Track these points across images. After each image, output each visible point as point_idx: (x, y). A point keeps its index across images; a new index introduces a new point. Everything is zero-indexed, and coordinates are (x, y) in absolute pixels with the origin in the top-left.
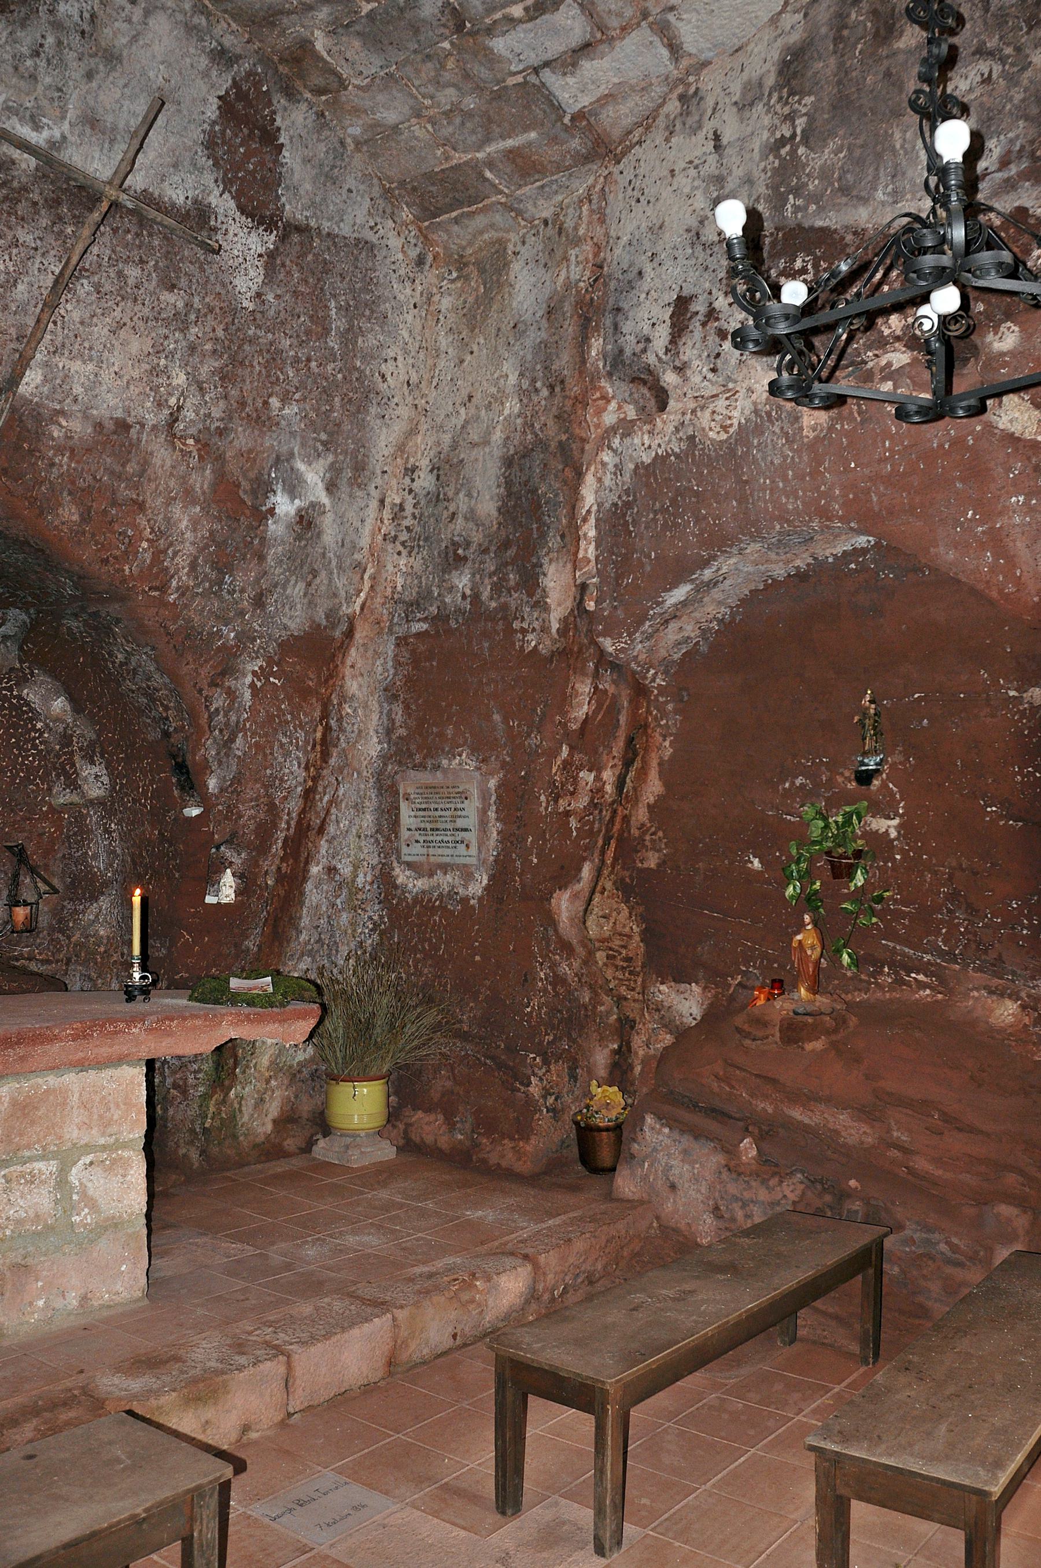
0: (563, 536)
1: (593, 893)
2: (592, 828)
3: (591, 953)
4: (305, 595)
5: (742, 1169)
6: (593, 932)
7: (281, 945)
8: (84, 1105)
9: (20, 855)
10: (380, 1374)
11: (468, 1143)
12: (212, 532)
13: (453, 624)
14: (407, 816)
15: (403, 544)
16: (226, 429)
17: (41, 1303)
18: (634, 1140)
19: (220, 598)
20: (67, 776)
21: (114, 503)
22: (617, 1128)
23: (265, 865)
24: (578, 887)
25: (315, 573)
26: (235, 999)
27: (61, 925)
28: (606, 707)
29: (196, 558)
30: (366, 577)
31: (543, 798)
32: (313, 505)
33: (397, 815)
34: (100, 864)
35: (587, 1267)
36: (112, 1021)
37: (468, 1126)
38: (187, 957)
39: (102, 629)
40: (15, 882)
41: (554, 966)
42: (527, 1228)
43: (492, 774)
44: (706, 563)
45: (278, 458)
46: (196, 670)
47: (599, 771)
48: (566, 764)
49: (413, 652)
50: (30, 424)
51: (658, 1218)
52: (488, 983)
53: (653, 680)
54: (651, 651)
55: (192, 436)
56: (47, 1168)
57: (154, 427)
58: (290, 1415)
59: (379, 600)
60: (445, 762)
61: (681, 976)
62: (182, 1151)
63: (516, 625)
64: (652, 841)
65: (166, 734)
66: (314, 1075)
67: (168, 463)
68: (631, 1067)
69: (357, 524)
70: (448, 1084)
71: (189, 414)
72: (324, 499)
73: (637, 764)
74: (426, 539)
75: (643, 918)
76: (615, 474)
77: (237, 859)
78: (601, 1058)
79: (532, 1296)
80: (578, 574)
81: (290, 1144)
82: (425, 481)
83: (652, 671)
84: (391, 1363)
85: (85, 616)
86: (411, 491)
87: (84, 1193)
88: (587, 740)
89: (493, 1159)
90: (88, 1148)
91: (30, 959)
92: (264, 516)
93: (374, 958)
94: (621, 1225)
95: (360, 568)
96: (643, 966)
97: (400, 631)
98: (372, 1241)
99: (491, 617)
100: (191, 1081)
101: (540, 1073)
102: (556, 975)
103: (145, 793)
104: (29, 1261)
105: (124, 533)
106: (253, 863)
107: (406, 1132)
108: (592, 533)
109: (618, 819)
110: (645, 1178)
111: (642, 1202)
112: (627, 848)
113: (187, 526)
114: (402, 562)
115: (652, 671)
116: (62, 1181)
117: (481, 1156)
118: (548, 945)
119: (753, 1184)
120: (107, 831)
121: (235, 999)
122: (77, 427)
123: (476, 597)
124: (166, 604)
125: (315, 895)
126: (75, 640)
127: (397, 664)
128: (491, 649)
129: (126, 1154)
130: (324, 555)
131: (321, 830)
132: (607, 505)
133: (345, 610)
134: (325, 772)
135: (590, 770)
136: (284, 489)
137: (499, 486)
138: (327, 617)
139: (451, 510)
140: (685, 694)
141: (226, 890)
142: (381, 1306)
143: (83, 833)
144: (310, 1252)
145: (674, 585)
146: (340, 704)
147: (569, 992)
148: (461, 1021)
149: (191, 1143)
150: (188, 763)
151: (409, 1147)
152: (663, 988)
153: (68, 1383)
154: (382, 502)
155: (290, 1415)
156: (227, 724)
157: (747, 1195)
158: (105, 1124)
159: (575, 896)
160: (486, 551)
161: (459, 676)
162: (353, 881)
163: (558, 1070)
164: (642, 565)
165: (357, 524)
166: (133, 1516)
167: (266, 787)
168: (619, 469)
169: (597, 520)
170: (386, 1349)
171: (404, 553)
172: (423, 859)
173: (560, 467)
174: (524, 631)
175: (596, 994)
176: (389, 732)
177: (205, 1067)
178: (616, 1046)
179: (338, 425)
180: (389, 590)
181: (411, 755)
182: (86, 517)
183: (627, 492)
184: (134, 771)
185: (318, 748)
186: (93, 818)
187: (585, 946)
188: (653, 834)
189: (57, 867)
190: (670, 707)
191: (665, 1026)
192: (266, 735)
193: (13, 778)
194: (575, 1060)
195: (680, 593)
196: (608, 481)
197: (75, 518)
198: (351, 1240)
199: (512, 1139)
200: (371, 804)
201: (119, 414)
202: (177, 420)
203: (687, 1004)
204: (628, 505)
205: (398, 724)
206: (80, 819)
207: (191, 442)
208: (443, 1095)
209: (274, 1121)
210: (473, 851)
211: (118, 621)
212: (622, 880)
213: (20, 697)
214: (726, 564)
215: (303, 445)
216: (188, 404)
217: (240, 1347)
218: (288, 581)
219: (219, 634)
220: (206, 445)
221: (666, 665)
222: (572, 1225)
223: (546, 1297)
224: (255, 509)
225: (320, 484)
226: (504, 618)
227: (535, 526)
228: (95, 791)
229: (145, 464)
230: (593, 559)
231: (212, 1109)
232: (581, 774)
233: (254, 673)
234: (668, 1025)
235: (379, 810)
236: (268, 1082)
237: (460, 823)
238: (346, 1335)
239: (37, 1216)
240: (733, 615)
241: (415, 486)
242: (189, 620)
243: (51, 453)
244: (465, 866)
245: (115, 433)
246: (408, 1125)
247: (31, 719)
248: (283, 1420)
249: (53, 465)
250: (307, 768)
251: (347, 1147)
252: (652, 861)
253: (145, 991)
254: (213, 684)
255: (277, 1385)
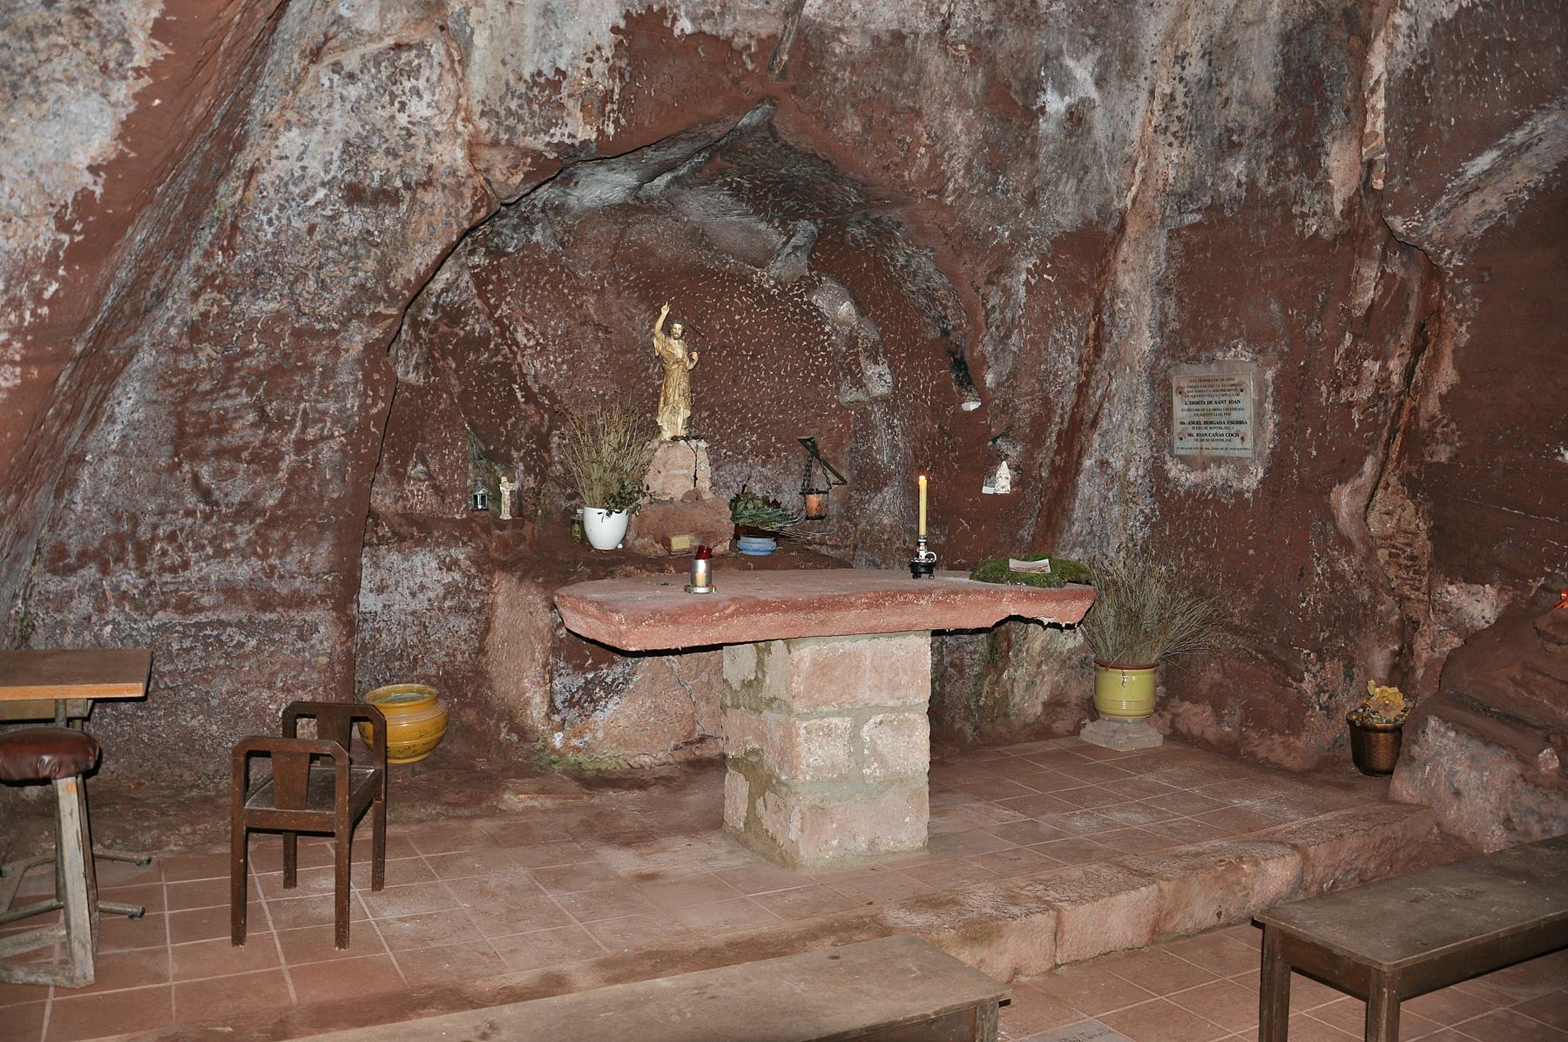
0: (1347, 112)
1: (1375, 488)
2: (1376, 421)
3: (1372, 551)
4: (1077, 191)
5: (1540, 780)
6: (1374, 528)
7: (1054, 535)
8: (875, 669)
9: (811, 447)
10: (1145, 940)
11: (1236, 736)
12: (985, 134)
13: (1228, 213)
14: (1180, 410)
15: (1174, 134)
16: (995, 31)
17: (835, 842)
18: (1415, 742)
19: (995, 198)
20: (854, 376)
21: (893, 112)
22: (1396, 731)
23: (1040, 458)
24: (1359, 482)
25: (1086, 169)
26: (1015, 577)
27: (848, 514)
28: (1394, 291)
29: (971, 160)
30: (1137, 171)
31: (1323, 388)
32: (1082, 101)
33: (1170, 409)
34: (884, 458)
35: (1359, 864)
36: (902, 592)
37: (1236, 719)
38: (972, 540)
39: (883, 234)
40: (808, 474)
41: (1331, 562)
42: (1296, 821)
43: (1268, 365)
44: (1517, 124)
45: (1047, 56)
46: (973, 269)
47: (1385, 361)
48: (1349, 353)
49: (1186, 244)
50: (814, 43)
51: (1438, 825)
52: (1261, 577)
53: (1449, 261)
54: (1447, 228)
55: (963, 42)
56: (842, 723)
57: (928, 36)
58: (1057, 966)
59: (1151, 193)
60: (1219, 354)
61: (1473, 576)
62: (957, 726)
63: (1296, 210)
64: (1443, 433)
65: (945, 332)
66: (1083, 663)
67: (942, 69)
68: (1413, 670)
69: (1127, 117)
70: (1218, 677)
71: (960, 21)
72: (1094, 94)
73: (1428, 352)
74: (1198, 128)
75: (1430, 515)
76: (1409, 36)
77: (1014, 451)
78: (1380, 659)
79: (1300, 884)
80: (1364, 150)
81: (1059, 726)
82: (1196, 68)
83: (1448, 251)
84: (1155, 931)
85: (869, 223)
86: (1181, 79)
87: (874, 749)
88: (1372, 329)
89: (1262, 753)
90: (879, 709)
91: (821, 544)
92: (1034, 114)
93: (1144, 550)
94: (1397, 827)
95: (1131, 161)
96: (1430, 565)
97: (1173, 224)
98: (1138, 819)
99: (1268, 204)
100: (967, 661)
101: (1314, 670)
102: (1334, 572)
103: (925, 389)
104: (826, 805)
105: (904, 140)
106: (1029, 455)
107: (1172, 722)
108: (1381, 105)
109: (1405, 412)
110: (1425, 782)
111: (1420, 806)
112: (1415, 441)
113: (961, 129)
114: (1174, 152)
115: (1448, 251)
116: (855, 737)
117: (1250, 749)
118: (1326, 540)
119: (1554, 798)
120: (890, 426)
121: (1015, 577)
122: (856, 42)
123: (1252, 184)
124: (944, 207)
125: (1087, 487)
126: (859, 246)
127: (1170, 257)
128: (1268, 236)
129: (912, 716)
130: (1094, 150)
131: (1094, 424)
132: (1399, 72)
133: (1117, 204)
134: (1097, 367)
135: (1375, 359)
136: (1053, 87)
137: (1276, 65)
138: (1099, 213)
139: (1225, 95)
140: (1485, 274)
141: (1002, 481)
142: (1148, 877)
143: (868, 427)
144: (1079, 824)
145: (1478, 152)
146: (1112, 300)
147: (1347, 589)
148: (1232, 615)
149: (966, 719)
150: (967, 359)
151: (1176, 736)
152: (1452, 588)
153: (861, 912)
154: (1152, 93)
155: (1057, 966)
156: (1003, 321)
157: (1544, 809)
158: (894, 688)
159: (1356, 491)
160: (1262, 135)
161: (1229, 266)
162: (1125, 475)
163: (1333, 667)
164: (1438, 133)
165: (1127, 117)
166: (925, 1016)
167: (1040, 382)
168: (1414, 30)
169: (1387, 90)
170: (1151, 917)
171: (1176, 143)
172: (1197, 452)
173: (1345, 37)
174: (1304, 216)
175: (1376, 592)
176: (1162, 325)
177: (980, 649)
178: (1396, 647)
179: (1106, 18)
180: (1161, 183)
181: (1184, 349)
182: (867, 128)
183: (1423, 56)
184: (915, 369)
185: (1091, 343)
186: (877, 414)
187: (1365, 543)
188: (1446, 426)
189: (845, 460)
190: (1468, 289)
191: (1454, 629)
192: (1040, 331)
193: (805, 377)
194: (1351, 659)
195: (1484, 161)
196: (1400, 45)
197: (858, 128)
198: (1118, 816)
199: (1282, 734)
200: (1143, 399)
201: (894, 26)
202: (948, 27)
203: (1480, 606)
204: (1424, 69)
205: (1171, 317)
206: (865, 415)
207: (962, 47)
208: (1212, 687)
209: (1044, 704)
210: (1249, 444)
211: (899, 225)
212: (1409, 475)
213: (809, 303)
214: (1543, 123)
215: (1071, 41)
216: (958, 11)
217: (1013, 899)
218: (1060, 178)
219: (994, 233)
220: (977, 49)
221: (1464, 244)
222: (1344, 821)
223: (1314, 888)
224: (1026, 108)
225: (1090, 81)
226: (1283, 204)
227: (1316, 103)
228: (880, 389)
229: (920, 72)
230: (1382, 132)
231: (986, 689)
232: (1366, 364)
233: (1028, 270)
234: (1456, 628)
235: (1152, 404)
236: (1039, 665)
237: (1235, 416)
238: (1113, 900)
239: (833, 765)
240: (1548, 182)
241: (1186, 73)
242: (966, 221)
243: (834, 69)
244: (1239, 459)
245: (891, 44)
246: (1175, 715)
247: (820, 324)
248: (1050, 970)
249: (836, 80)
250: (1080, 363)
251: (1115, 732)
252: (1443, 455)
253: (929, 568)
254: (990, 282)
255: (1047, 937)
